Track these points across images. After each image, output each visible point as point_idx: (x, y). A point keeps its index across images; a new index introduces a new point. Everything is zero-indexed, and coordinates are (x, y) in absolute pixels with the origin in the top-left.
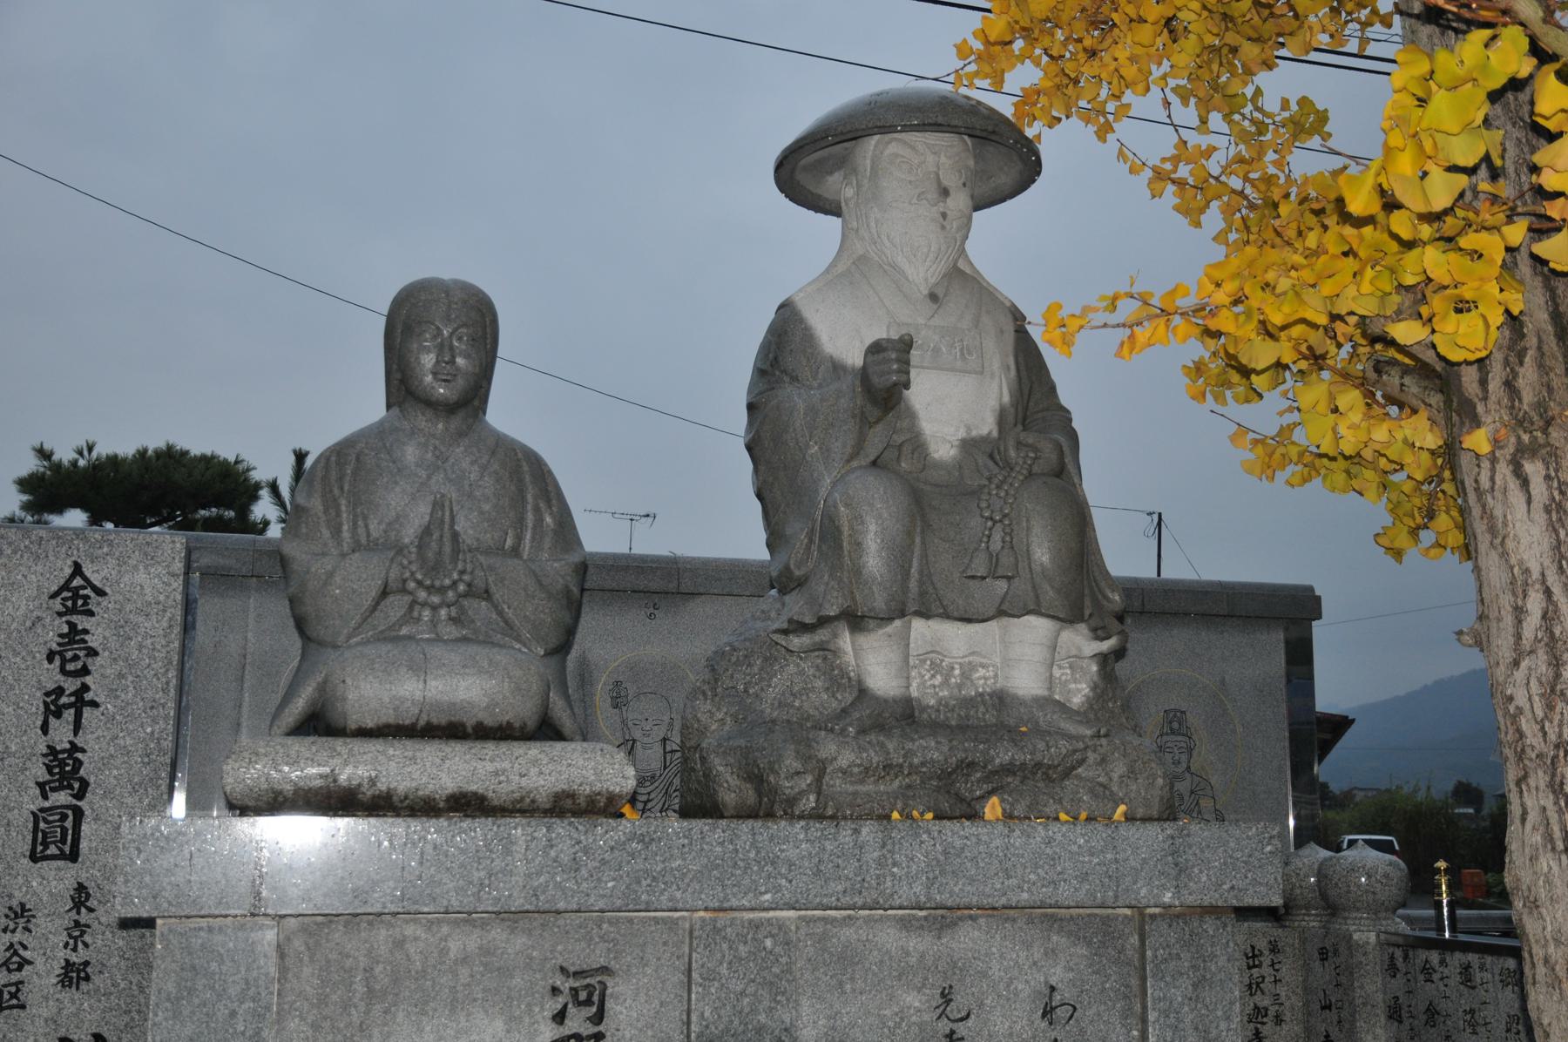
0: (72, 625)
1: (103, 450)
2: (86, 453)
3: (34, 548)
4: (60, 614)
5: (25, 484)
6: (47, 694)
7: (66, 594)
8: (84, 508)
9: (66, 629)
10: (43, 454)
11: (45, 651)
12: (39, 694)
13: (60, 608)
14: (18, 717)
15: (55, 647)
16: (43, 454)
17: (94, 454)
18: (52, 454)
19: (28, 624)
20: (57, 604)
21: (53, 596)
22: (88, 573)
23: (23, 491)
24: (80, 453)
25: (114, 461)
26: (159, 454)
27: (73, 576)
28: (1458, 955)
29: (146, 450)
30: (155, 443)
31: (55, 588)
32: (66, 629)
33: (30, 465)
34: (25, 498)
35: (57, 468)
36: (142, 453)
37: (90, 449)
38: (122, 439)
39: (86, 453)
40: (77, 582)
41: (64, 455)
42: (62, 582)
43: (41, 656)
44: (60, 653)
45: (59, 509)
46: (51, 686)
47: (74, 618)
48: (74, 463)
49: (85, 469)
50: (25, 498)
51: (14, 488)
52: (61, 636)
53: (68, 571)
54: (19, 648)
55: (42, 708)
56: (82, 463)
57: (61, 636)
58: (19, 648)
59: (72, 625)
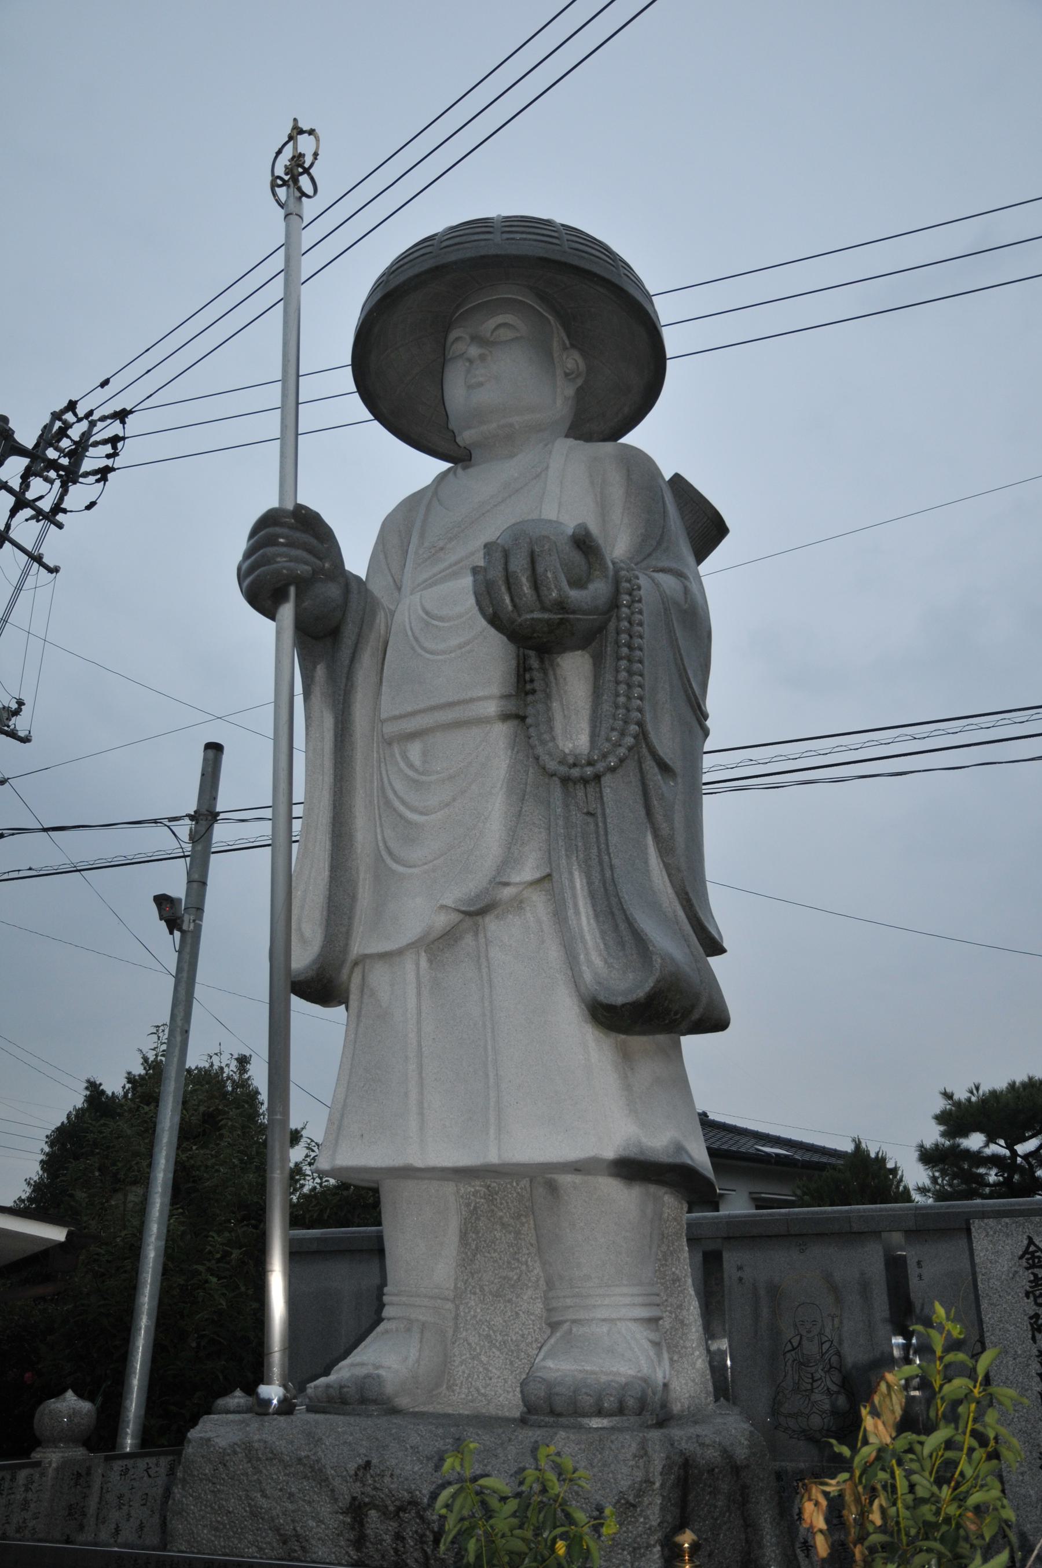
0: (1035, 1275)
1: (985, 1088)
2: (975, 1092)
3: (1005, 1230)
4: (1027, 1269)
5: (941, 1118)
6: (1031, 1318)
7: (1028, 1256)
8: (982, 1131)
9: (1032, 1278)
10: (948, 1096)
11: (1023, 1291)
12: (1026, 1318)
13: (1025, 1264)
14: (1018, 1333)
15: (1028, 1288)
16: (948, 1096)
17: (981, 1092)
18: (953, 1094)
19: (1011, 1275)
20: (1024, 1262)
21: (1021, 1257)
22: (1037, 1243)
23: (940, 1124)
24: (971, 1092)
25: (994, 1094)
26: (1024, 1085)
27: (1028, 1247)
28: (120, 1462)
29: (1014, 1083)
30: (1020, 1077)
31: (1020, 1253)
32: (1032, 1278)
33: (940, 1105)
34: (942, 1128)
35: (958, 1104)
36: (1012, 1086)
37: (977, 1088)
38: (996, 1078)
39: (975, 1092)
40: (1032, 1248)
41: (961, 1095)
42: (1024, 1248)
43: (1022, 1295)
44: (1032, 1292)
45: (966, 1135)
46: (1032, 1313)
47: (1036, 1271)
48: (969, 1100)
49: (977, 1103)
50: (942, 1128)
51: (933, 1122)
52: (1030, 1282)
53: (1026, 1242)
54: (1009, 1290)
55: (1029, 1327)
56: (974, 1099)
57: (1030, 1282)
58: (1009, 1290)
59: (1035, 1275)
